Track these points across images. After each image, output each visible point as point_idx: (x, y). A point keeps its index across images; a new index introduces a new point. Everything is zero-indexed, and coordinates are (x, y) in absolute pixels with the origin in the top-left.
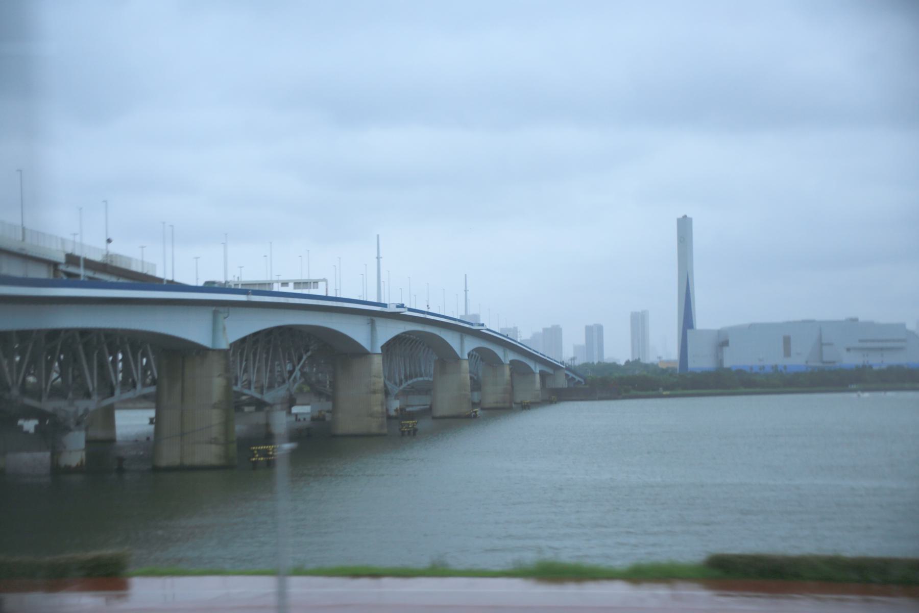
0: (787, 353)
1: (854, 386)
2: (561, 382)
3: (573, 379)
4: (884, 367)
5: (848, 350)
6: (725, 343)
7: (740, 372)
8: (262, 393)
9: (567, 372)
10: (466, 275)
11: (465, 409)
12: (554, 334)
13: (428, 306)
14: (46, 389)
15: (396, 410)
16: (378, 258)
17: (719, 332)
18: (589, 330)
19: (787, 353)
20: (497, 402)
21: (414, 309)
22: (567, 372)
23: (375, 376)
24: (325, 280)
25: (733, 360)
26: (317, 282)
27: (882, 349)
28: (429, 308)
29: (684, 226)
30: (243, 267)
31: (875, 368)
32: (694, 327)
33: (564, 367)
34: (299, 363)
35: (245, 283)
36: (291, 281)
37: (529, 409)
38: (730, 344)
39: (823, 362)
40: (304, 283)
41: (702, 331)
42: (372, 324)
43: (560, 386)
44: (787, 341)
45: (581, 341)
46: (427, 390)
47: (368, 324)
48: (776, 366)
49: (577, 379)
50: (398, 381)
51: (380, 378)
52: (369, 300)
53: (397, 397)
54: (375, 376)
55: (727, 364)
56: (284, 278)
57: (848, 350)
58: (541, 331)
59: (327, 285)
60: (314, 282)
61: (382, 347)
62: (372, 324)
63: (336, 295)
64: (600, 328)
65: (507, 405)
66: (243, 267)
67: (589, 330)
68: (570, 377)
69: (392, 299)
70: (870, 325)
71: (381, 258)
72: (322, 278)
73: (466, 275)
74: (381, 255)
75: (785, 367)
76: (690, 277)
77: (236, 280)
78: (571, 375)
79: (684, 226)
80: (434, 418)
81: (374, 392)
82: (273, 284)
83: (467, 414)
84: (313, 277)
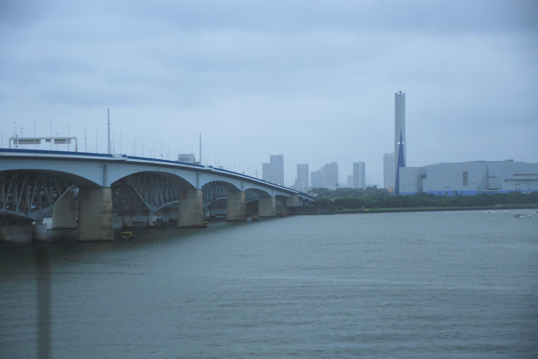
0: (465, 183)
1: (498, 206)
2: (296, 203)
3: (306, 200)
4: (529, 192)
5: (506, 181)
6: (424, 176)
7: (431, 196)
8: (27, 213)
9: (300, 196)
10: (200, 134)
11: (199, 222)
12: (332, 169)
13: (162, 156)
14: (5, 202)
15: (154, 222)
16: (109, 124)
17: (421, 168)
18: (355, 165)
19: (465, 183)
20: (236, 217)
21: (142, 158)
22: (300, 196)
23: (105, 202)
24: (75, 138)
25: (429, 187)
26: (70, 139)
27: (529, 180)
28: (162, 156)
29: (400, 99)
30: (23, 128)
31: (523, 193)
32: (405, 165)
33: (298, 193)
34: (62, 193)
35: (31, 139)
36: (53, 138)
37: (257, 221)
38: (427, 176)
39: (490, 189)
40: (31, 140)
41: (409, 168)
42: (105, 167)
43: (294, 205)
44: (465, 175)
45: (295, 176)
46: (176, 209)
47: (100, 167)
48: (456, 191)
49: (311, 200)
50: (157, 202)
51: (109, 203)
52: (98, 153)
53: (155, 214)
54: (105, 202)
55: (425, 190)
56: (48, 136)
57: (506, 181)
58: (324, 166)
59: (76, 141)
60: (68, 140)
61: (112, 185)
62: (105, 167)
63: (69, 150)
64: (363, 165)
65: (243, 218)
66: (23, 128)
67: (355, 165)
68: (304, 199)
69: (118, 152)
70: (522, 164)
71: (111, 124)
72: (73, 137)
73: (200, 134)
74: (110, 122)
75: (462, 192)
76: (402, 132)
77: (15, 137)
78: (305, 197)
79: (400, 99)
80: (179, 228)
81: (105, 213)
82: (40, 140)
83: (200, 225)
84: (38, 136)
